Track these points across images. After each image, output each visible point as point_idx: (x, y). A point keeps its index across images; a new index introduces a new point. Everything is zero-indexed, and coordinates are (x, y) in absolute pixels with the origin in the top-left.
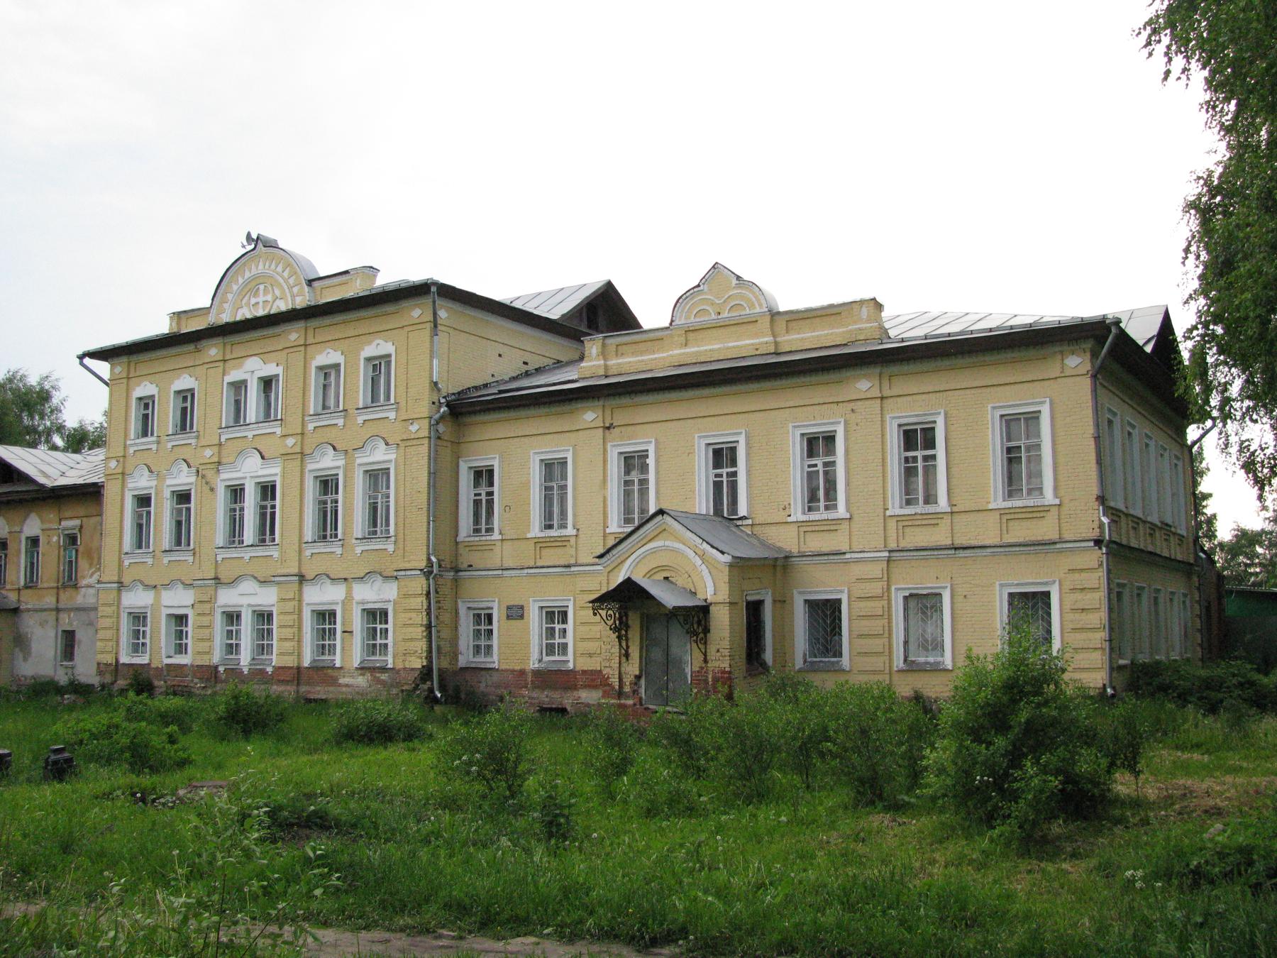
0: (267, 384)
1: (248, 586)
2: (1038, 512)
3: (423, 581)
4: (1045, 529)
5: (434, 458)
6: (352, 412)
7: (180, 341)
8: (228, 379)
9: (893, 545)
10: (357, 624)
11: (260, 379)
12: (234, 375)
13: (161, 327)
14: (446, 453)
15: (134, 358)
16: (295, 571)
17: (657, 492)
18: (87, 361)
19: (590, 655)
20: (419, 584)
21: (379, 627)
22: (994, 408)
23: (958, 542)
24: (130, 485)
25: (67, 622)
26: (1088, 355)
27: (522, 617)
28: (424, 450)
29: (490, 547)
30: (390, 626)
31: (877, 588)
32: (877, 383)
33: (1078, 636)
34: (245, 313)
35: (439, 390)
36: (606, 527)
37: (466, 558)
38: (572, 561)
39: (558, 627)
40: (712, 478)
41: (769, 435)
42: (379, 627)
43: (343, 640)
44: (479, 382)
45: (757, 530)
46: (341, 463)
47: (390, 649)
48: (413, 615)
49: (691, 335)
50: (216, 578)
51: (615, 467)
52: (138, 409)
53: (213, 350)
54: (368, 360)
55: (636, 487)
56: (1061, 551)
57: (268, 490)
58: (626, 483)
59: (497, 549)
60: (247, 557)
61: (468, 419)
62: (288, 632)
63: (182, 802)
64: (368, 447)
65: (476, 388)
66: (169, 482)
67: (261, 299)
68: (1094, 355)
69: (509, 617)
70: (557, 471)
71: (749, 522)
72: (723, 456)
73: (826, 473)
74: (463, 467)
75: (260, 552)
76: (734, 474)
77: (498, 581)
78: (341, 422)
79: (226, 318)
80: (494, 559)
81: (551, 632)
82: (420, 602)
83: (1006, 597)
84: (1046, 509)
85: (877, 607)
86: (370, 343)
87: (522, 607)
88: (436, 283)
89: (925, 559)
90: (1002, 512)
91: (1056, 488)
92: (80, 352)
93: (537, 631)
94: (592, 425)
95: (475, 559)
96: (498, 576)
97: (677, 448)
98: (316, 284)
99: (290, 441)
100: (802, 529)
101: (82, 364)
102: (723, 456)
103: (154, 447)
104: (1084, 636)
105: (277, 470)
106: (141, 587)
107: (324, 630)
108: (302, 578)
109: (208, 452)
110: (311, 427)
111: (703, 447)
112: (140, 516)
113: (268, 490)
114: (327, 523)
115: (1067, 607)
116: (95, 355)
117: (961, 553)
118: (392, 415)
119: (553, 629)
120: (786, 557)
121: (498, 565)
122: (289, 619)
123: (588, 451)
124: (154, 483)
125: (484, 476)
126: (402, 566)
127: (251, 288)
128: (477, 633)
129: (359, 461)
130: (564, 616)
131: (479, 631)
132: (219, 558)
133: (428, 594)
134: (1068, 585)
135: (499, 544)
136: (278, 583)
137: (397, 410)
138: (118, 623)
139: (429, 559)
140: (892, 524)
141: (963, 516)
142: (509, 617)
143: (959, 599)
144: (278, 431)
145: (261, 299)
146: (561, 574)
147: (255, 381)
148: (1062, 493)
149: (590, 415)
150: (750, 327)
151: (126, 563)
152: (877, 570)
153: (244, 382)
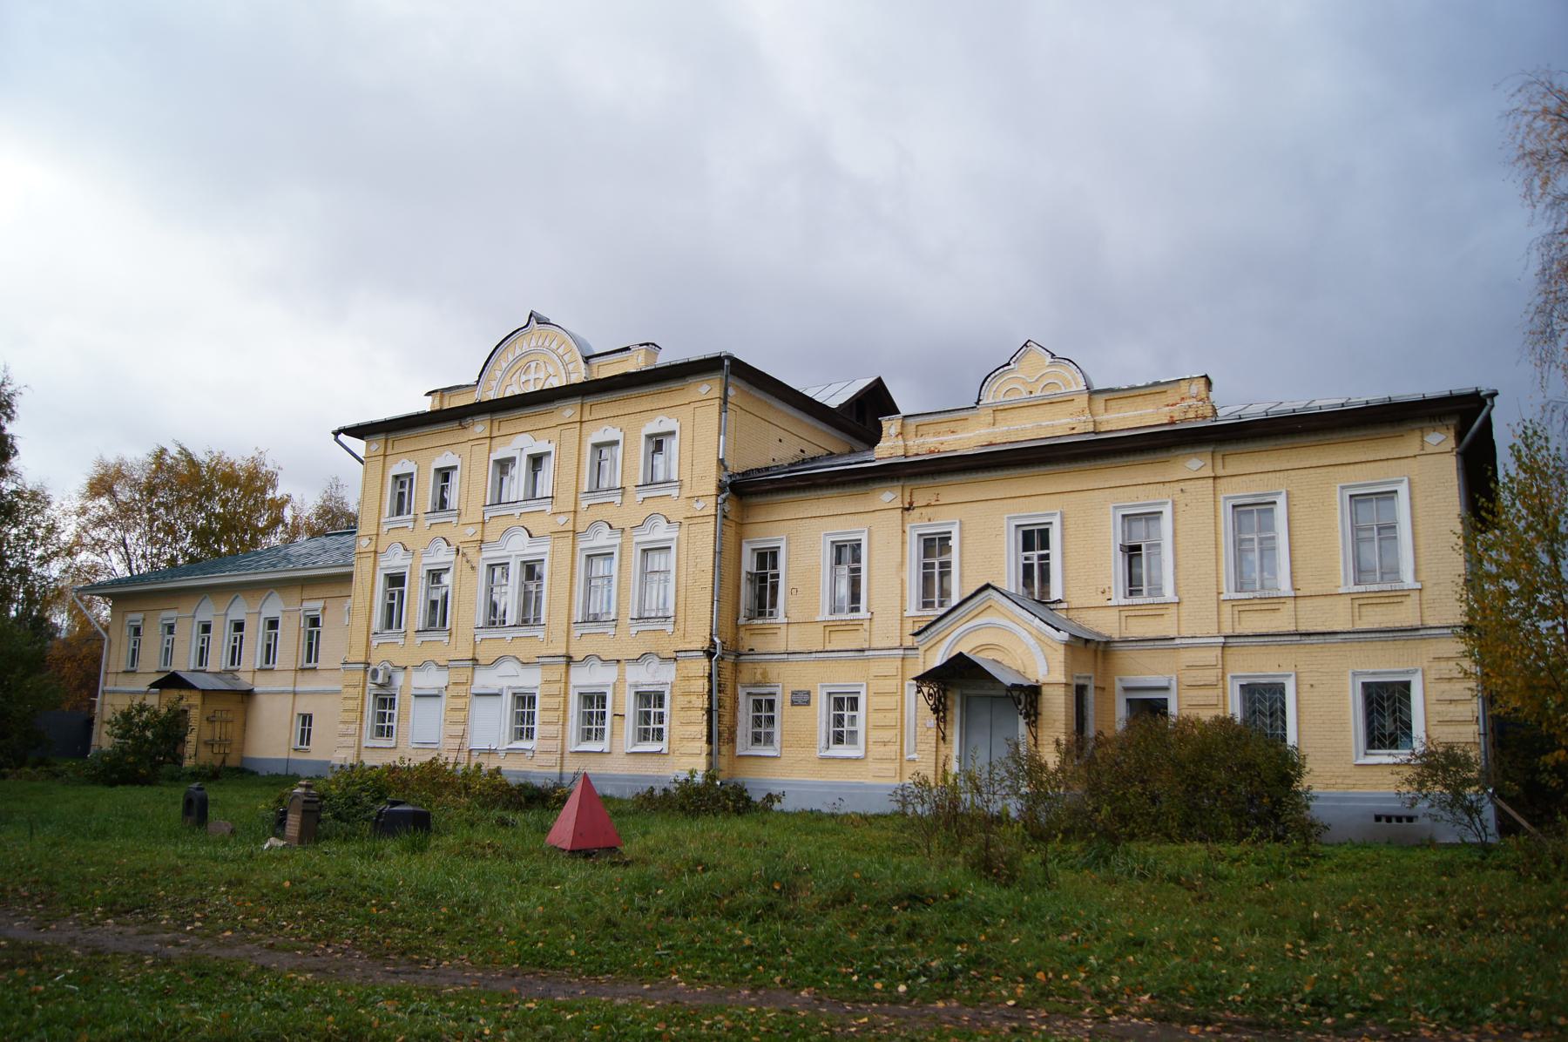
0: (536, 461)
1: (509, 667)
2: (1397, 596)
3: (705, 662)
4: (1405, 615)
5: (720, 537)
6: (630, 489)
7: (445, 417)
8: (496, 456)
9: (1229, 632)
10: (629, 706)
11: (530, 456)
12: (501, 453)
13: (426, 405)
14: (731, 532)
15: (590, 401)
16: (563, 652)
17: (961, 575)
18: (342, 437)
19: (885, 744)
20: (701, 666)
21: (653, 710)
22: (1343, 488)
23: (1302, 629)
24: (383, 565)
25: (304, 706)
26: (1452, 434)
27: (808, 703)
28: (710, 528)
29: (772, 631)
30: (666, 710)
31: (1211, 676)
32: (1209, 462)
33: (1446, 729)
34: (515, 390)
35: (726, 469)
36: (903, 610)
37: (748, 641)
38: (866, 646)
39: (847, 714)
40: (1022, 561)
41: (1086, 518)
42: (653, 710)
43: (612, 724)
44: (762, 465)
45: (1072, 614)
46: (675, 535)
47: (666, 734)
48: (694, 698)
49: (1000, 416)
50: (474, 659)
51: (914, 549)
52: (394, 488)
53: (480, 427)
54: (649, 437)
55: (937, 571)
56: (1422, 638)
57: (531, 571)
58: (926, 566)
59: (783, 631)
60: (509, 637)
61: (755, 500)
62: (552, 716)
63: (1297, 959)
64: (648, 525)
65: (758, 470)
66: (426, 561)
67: (532, 376)
68: (1459, 437)
69: (793, 703)
70: (847, 554)
71: (1064, 605)
72: (1034, 538)
73: (1041, 566)
74: (747, 550)
75: (524, 632)
76: (1047, 557)
77: (781, 665)
78: (618, 499)
79: (492, 395)
80: (779, 643)
81: (839, 720)
82: (701, 685)
83: (1359, 686)
84: (1405, 594)
85: (891, 702)
86: (652, 419)
87: (809, 693)
88: (730, 357)
89: (1265, 645)
90: (1354, 597)
91: (1416, 571)
92: (336, 429)
93: (824, 718)
94: (1438, 450)
95: (758, 643)
96: (783, 661)
97: (984, 528)
98: (592, 361)
99: (562, 519)
100: (1357, 602)
101: (336, 440)
102: (1034, 538)
103: (411, 525)
104: (1452, 729)
105: (547, 549)
106: (434, 668)
107: (591, 714)
108: (569, 660)
109: (470, 530)
110: (584, 504)
111: (1013, 529)
112: (392, 596)
113: (531, 571)
114: (392, 617)
115: (1433, 697)
116: (359, 431)
117: (1307, 640)
118: (675, 492)
119: (842, 717)
120: (1107, 643)
121: (783, 649)
122: (554, 702)
123: (883, 527)
124: (618, 541)
125: (767, 558)
126: (681, 647)
127: (523, 363)
128: (757, 721)
129: (637, 539)
130: (854, 704)
131: (759, 718)
132: (478, 639)
133: (710, 675)
134: (1432, 675)
135: (784, 627)
136: (543, 664)
137: (681, 487)
138: (566, 702)
139: (712, 640)
140: (1226, 608)
141: (1308, 601)
142: (793, 703)
143: (1305, 688)
144: (549, 509)
145: (532, 376)
146: (853, 659)
147: (525, 459)
148: (1423, 576)
149: (888, 496)
150: (1064, 406)
151: (375, 643)
152: (1212, 656)
153: (512, 460)
